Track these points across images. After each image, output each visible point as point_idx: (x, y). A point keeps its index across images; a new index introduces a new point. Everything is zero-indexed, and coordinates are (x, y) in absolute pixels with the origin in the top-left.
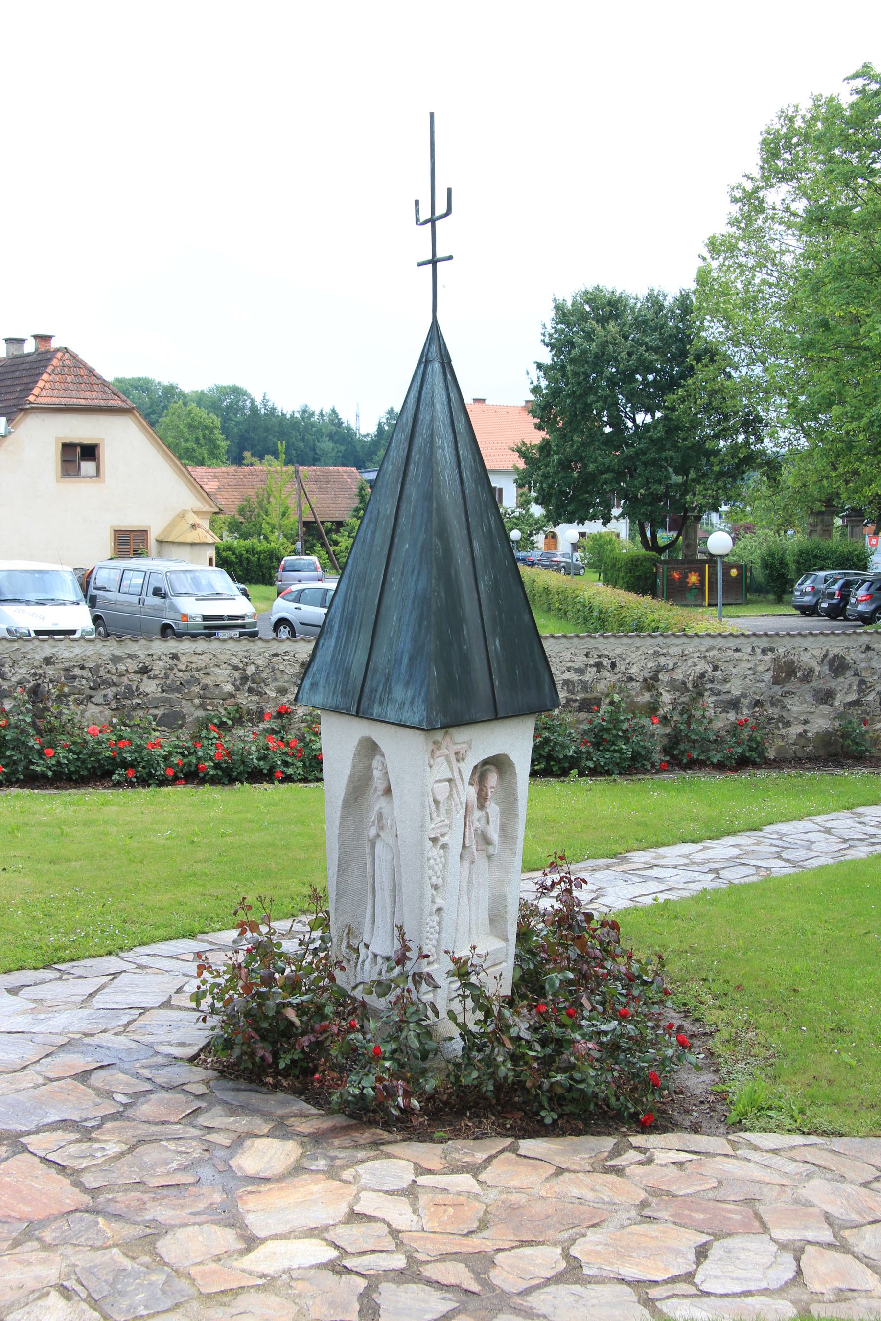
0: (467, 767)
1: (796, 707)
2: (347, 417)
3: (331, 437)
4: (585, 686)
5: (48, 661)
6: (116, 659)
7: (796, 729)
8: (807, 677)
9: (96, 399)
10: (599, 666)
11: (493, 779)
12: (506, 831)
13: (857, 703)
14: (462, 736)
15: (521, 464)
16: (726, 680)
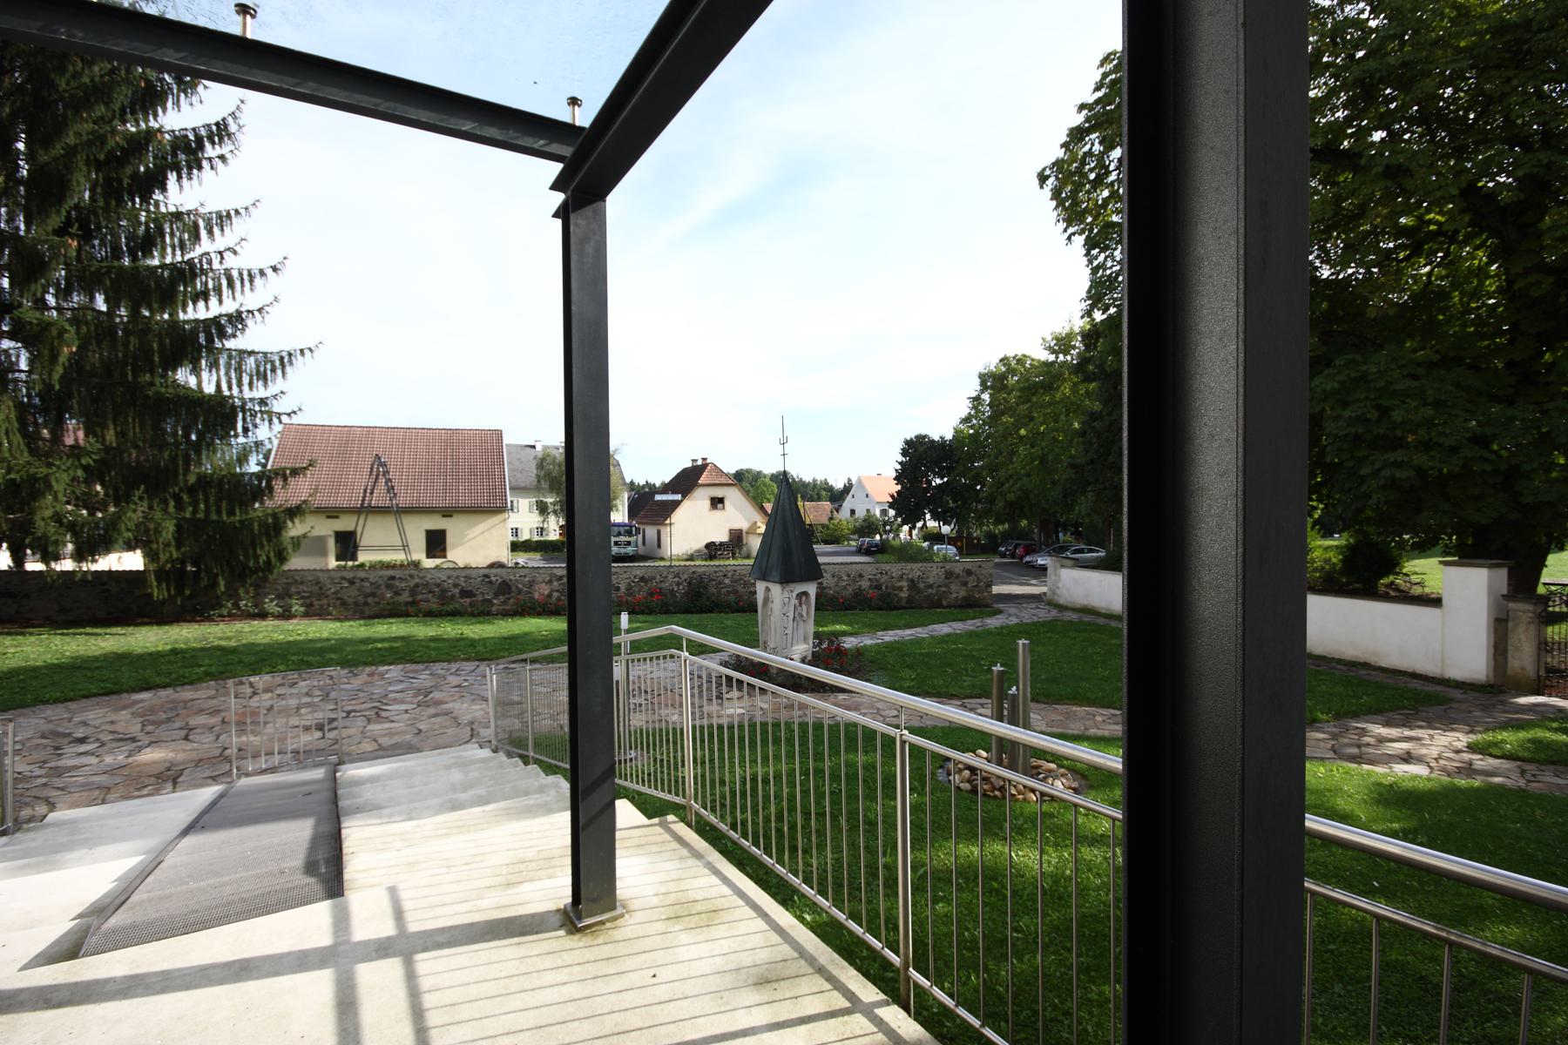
0: (794, 595)
1: (953, 587)
2: (831, 482)
3: (824, 489)
4: (876, 580)
5: (694, 573)
6: (715, 572)
7: (955, 595)
8: (958, 576)
9: (723, 480)
10: (881, 573)
11: (804, 598)
12: (808, 613)
13: (977, 586)
14: (792, 586)
15: (891, 500)
16: (928, 578)
